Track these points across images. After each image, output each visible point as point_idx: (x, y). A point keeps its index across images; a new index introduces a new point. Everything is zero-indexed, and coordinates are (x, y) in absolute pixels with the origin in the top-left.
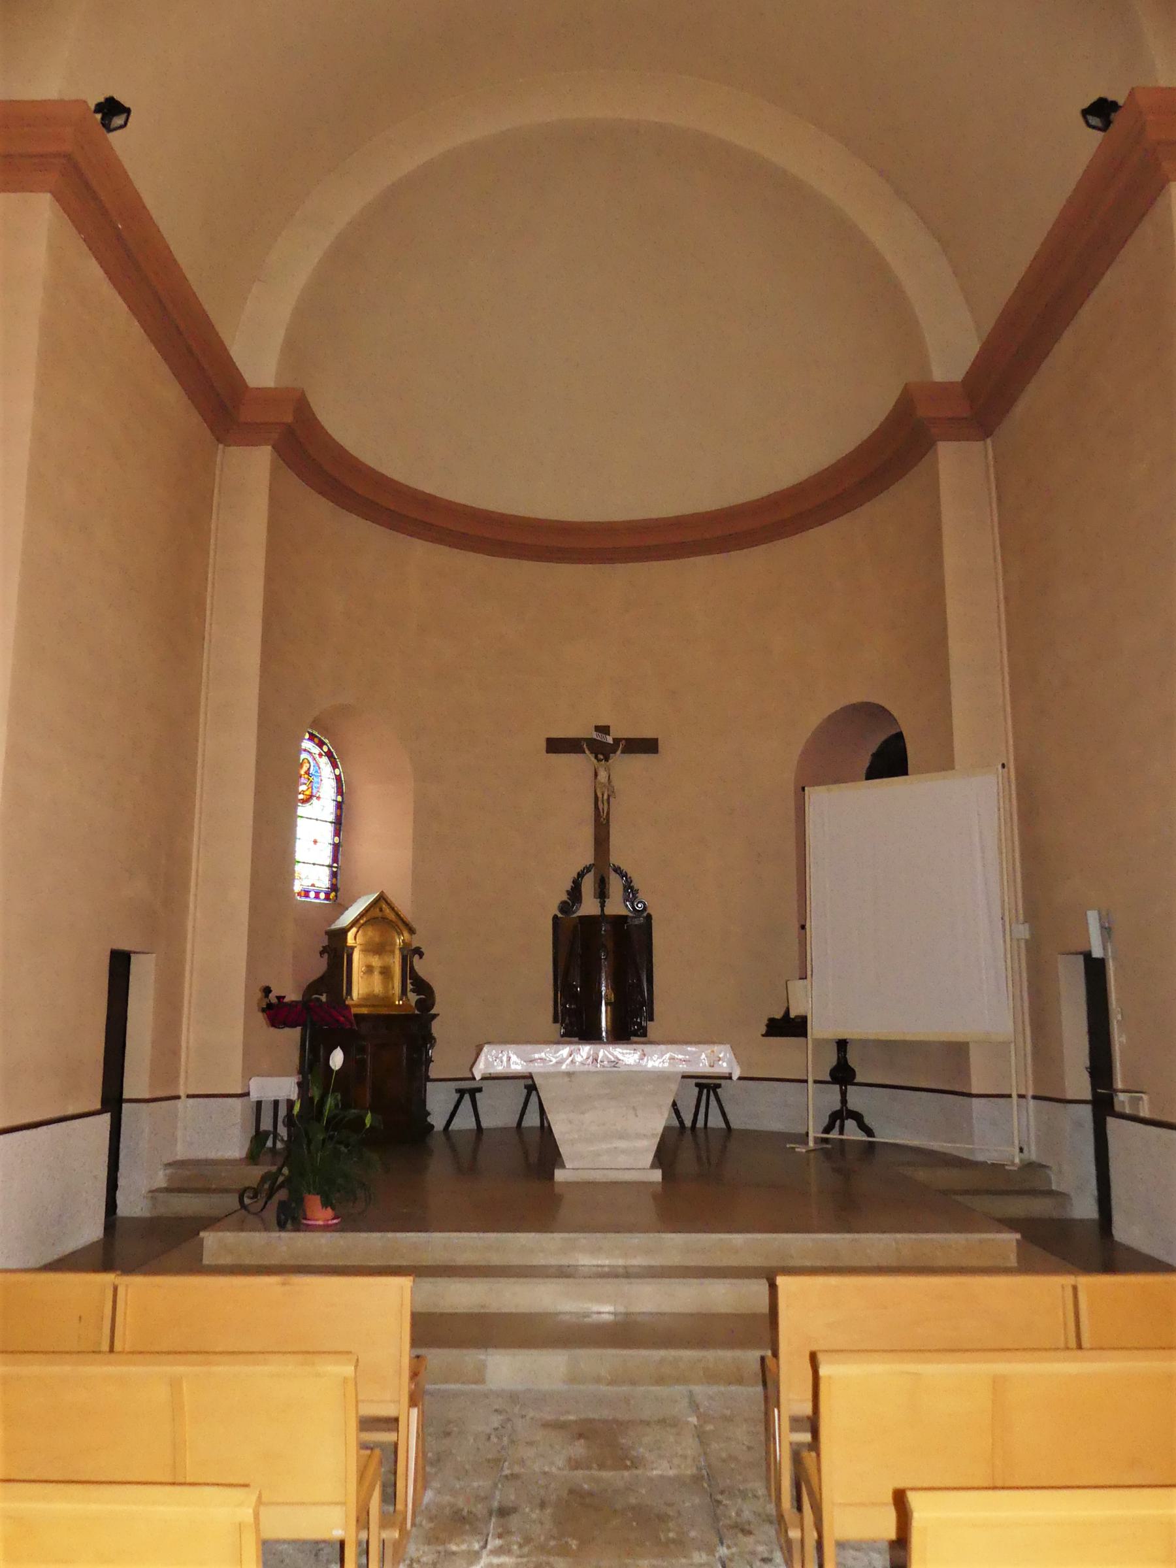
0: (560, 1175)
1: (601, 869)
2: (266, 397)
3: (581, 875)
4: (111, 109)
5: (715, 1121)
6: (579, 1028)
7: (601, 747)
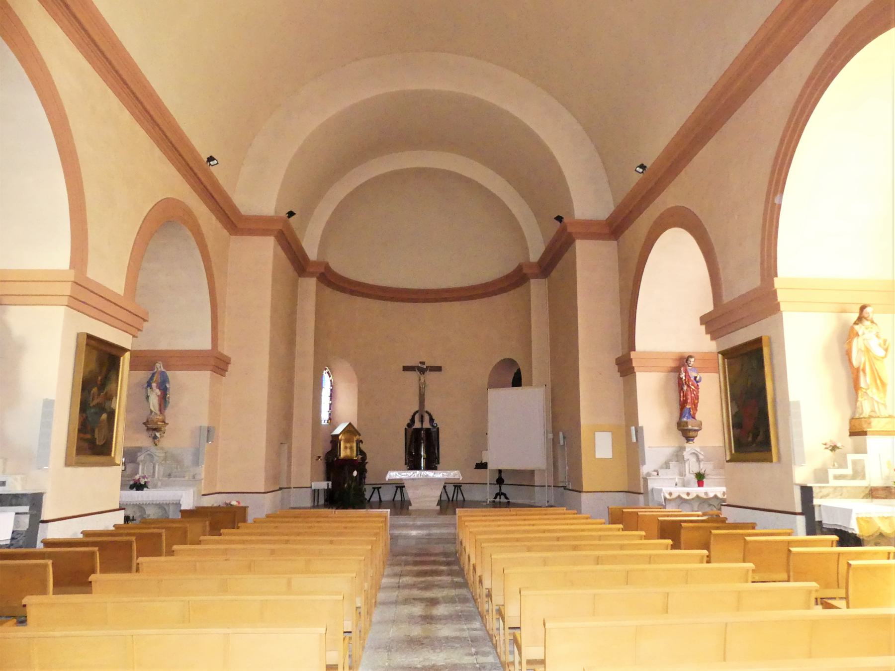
0: (410, 508)
1: (421, 412)
2: (317, 264)
3: (415, 414)
4: (291, 214)
5: (460, 497)
6: (413, 465)
7: (422, 370)
